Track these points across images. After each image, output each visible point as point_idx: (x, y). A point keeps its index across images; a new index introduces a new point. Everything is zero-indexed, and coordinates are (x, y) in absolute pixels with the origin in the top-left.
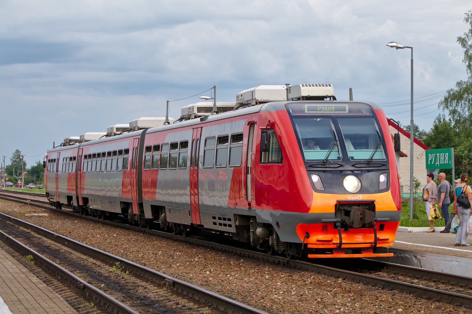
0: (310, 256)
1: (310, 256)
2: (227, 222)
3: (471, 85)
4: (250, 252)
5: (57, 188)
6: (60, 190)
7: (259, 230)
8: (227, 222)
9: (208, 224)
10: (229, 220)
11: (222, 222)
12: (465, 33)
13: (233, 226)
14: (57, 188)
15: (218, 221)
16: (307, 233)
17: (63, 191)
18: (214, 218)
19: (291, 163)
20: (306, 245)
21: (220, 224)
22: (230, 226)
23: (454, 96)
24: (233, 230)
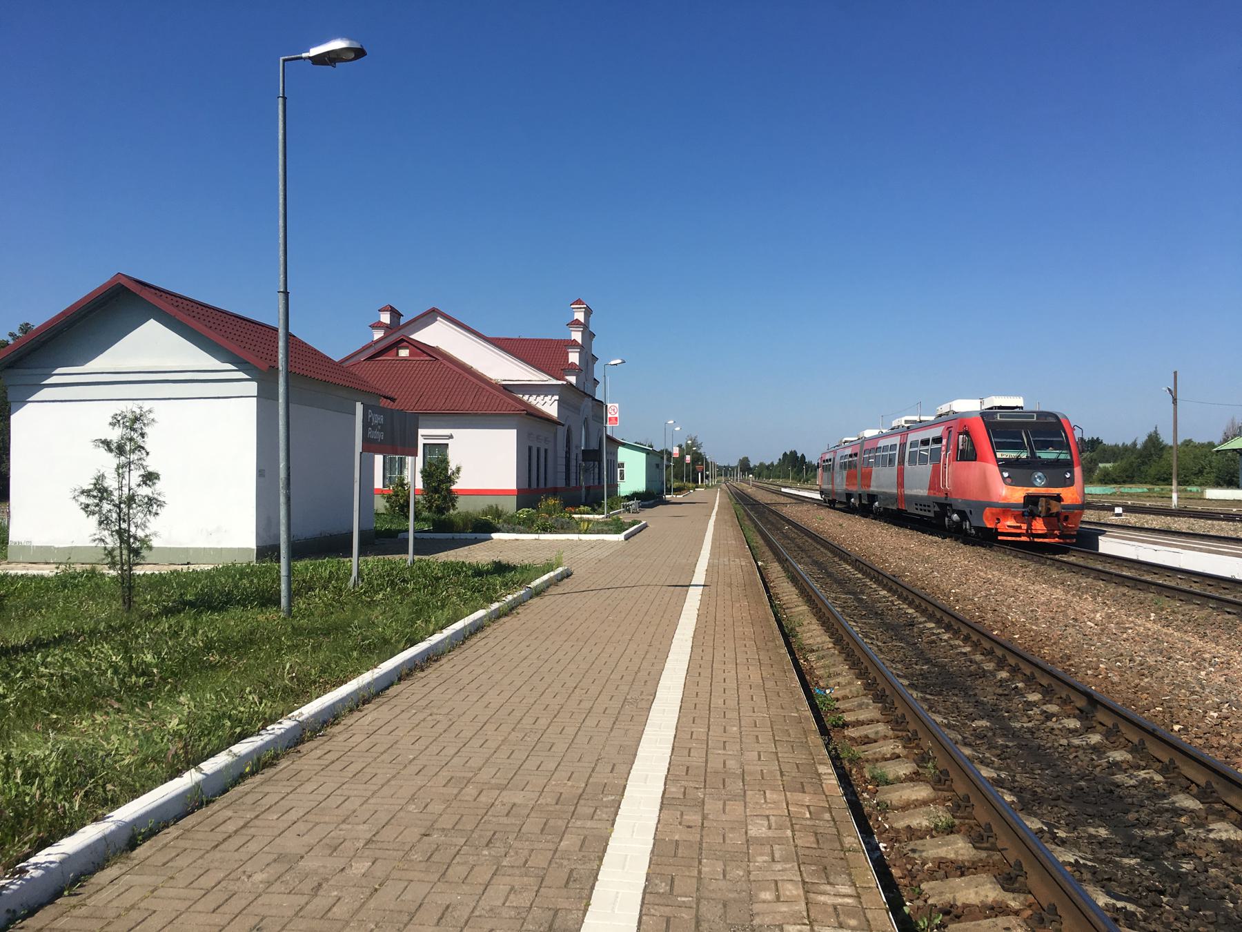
0: (1000, 538)
1: (1000, 538)
2: (927, 508)
3: (753, 931)
4: (546, 458)
5: (901, 484)
6: (907, 492)
7: (955, 517)
8: (927, 508)
9: (912, 509)
10: (929, 506)
11: (923, 507)
12: (110, 424)
13: (932, 511)
14: (901, 484)
15: (919, 507)
16: (998, 519)
17: (915, 492)
18: (916, 504)
19: (451, 325)
20: (996, 529)
21: (921, 510)
22: (929, 511)
23: (136, 552)
24: (931, 514)
